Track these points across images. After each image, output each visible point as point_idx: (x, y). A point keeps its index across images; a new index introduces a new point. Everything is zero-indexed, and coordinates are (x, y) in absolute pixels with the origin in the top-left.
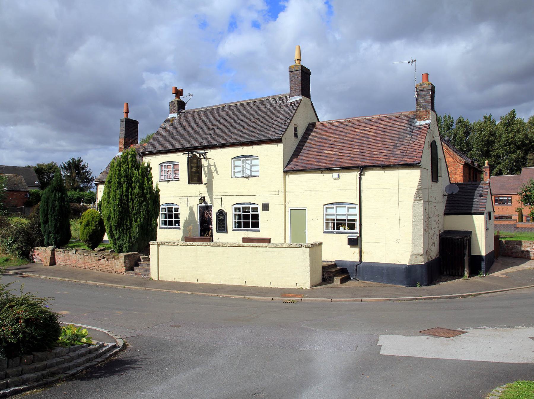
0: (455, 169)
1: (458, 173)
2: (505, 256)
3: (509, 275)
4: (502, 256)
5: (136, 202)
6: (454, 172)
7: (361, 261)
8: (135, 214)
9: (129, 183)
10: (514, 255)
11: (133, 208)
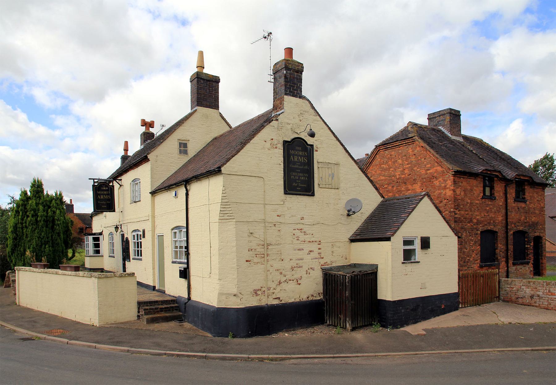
0: (444, 180)
1: (448, 186)
2: (508, 302)
3: (430, 332)
4: (504, 301)
5: (29, 230)
6: (443, 185)
7: (189, 298)
8: (29, 241)
9: (25, 211)
10: (520, 301)
11: (27, 235)
